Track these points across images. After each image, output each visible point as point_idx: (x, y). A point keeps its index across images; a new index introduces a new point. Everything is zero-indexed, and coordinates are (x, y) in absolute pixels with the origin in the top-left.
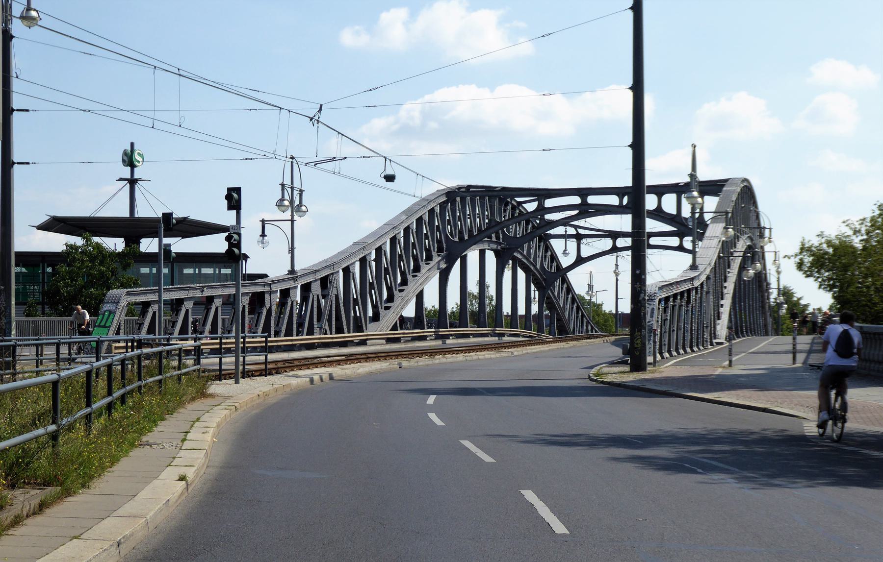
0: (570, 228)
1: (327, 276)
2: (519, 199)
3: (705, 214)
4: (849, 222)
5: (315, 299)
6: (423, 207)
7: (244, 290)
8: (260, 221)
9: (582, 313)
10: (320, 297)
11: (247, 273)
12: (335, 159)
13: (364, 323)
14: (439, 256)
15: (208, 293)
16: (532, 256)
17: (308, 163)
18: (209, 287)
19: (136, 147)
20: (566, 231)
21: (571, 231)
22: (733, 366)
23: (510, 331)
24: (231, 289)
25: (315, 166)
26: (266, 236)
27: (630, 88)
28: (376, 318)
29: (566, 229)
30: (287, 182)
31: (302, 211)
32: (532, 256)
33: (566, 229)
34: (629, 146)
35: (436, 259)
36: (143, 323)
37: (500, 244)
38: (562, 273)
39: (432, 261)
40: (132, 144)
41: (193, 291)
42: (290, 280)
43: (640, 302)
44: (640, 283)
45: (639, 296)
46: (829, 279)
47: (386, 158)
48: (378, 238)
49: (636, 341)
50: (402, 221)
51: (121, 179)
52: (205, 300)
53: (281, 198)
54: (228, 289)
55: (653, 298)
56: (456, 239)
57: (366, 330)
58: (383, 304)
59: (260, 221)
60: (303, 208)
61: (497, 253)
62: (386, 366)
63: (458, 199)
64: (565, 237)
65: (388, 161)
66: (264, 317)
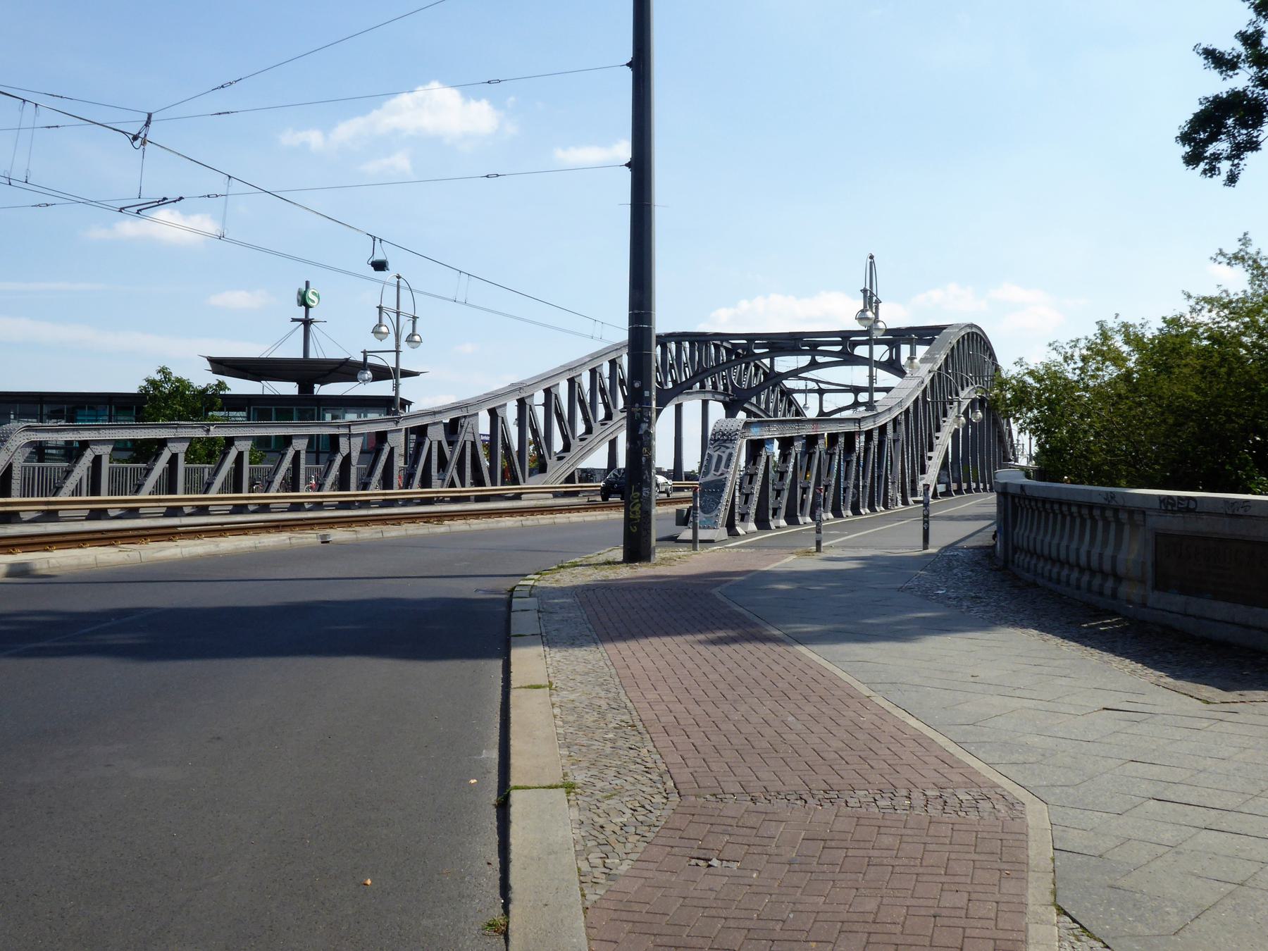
0: (810, 382)
4: (1056, 344)
12: (166, 201)
17: (123, 208)
19: (311, 286)
22: (822, 550)
25: (138, 213)
27: (628, 65)
30: (868, 287)
31: (415, 341)
36: (756, 474)
37: (729, 395)
40: (307, 284)
43: (640, 437)
44: (641, 404)
45: (638, 427)
46: (1036, 420)
47: (374, 239)
48: (543, 380)
49: (633, 507)
51: (294, 320)
53: (378, 323)
60: (417, 338)
64: (806, 391)
65: (377, 241)
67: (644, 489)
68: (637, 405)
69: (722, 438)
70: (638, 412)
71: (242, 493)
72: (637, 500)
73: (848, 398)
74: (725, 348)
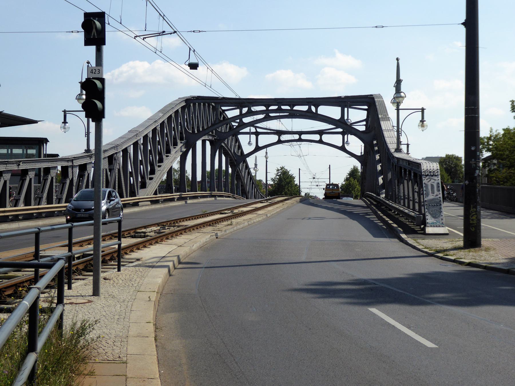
1: (113, 155)
2: (223, 108)
3: (400, 110)
5: (105, 172)
6: (172, 108)
7: (52, 164)
8: (63, 111)
9: (253, 181)
10: (108, 170)
11: (47, 153)
12: (164, 33)
13: (136, 190)
14: (181, 143)
15: (23, 167)
16: (229, 145)
18: (24, 162)
20: (250, 130)
21: (253, 130)
23: (219, 193)
24: (42, 163)
26: (67, 123)
28: (144, 185)
29: (250, 128)
32: (229, 145)
33: (250, 128)
34: (462, 24)
35: (180, 145)
38: (243, 157)
39: (177, 146)
41: (10, 165)
42: (87, 157)
49: (472, 217)
50: (160, 117)
52: (20, 172)
54: (40, 163)
55: (436, 174)
56: (191, 132)
57: (138, 195)
58: (148, 175)
59: (63, 111)
61: (212, 143)
62: (209, 238)
63: (192, 105)
64: (250, 133)
66: (68, 186)
67: (478, 207)
68: (473, 160)
69: (430, 174)
70: (474, 164)
71: (31, 206)
72: (475, 213)
73: (326, 138)
74: (212, 105)
